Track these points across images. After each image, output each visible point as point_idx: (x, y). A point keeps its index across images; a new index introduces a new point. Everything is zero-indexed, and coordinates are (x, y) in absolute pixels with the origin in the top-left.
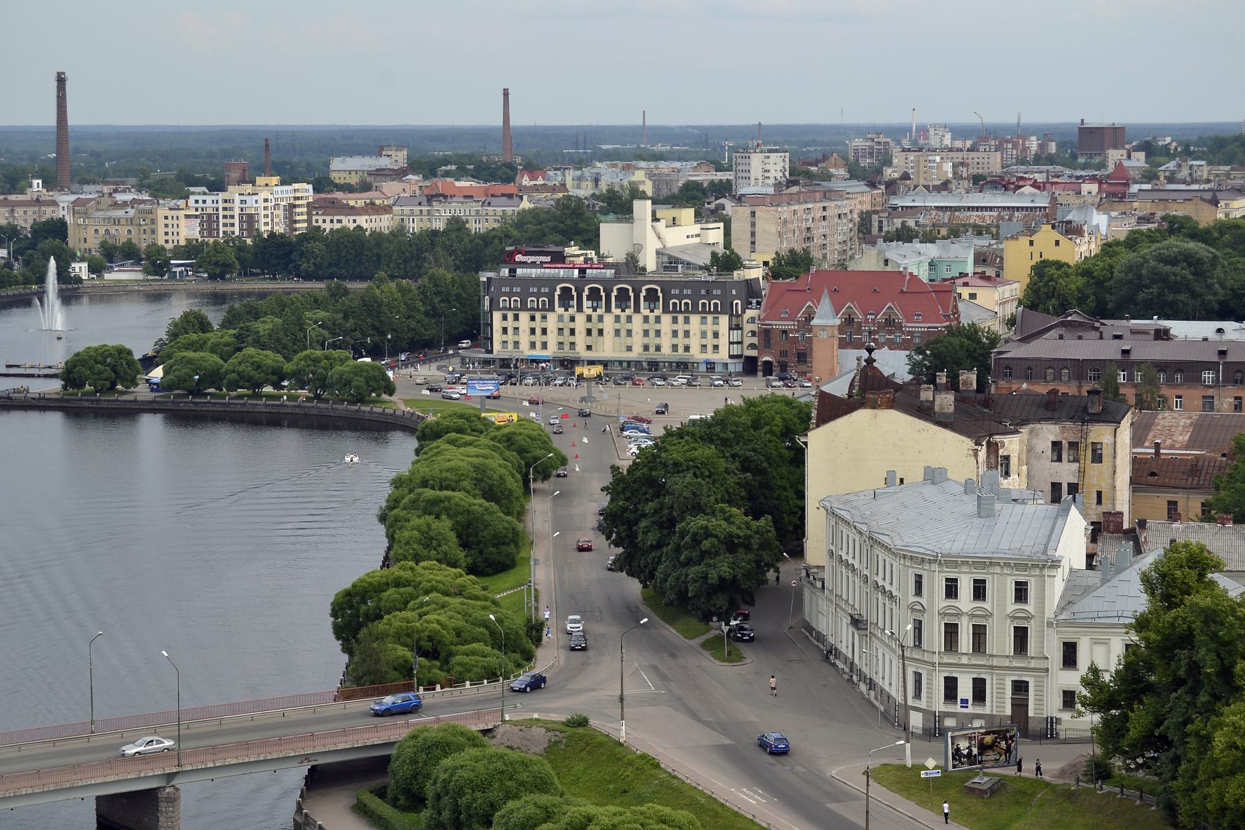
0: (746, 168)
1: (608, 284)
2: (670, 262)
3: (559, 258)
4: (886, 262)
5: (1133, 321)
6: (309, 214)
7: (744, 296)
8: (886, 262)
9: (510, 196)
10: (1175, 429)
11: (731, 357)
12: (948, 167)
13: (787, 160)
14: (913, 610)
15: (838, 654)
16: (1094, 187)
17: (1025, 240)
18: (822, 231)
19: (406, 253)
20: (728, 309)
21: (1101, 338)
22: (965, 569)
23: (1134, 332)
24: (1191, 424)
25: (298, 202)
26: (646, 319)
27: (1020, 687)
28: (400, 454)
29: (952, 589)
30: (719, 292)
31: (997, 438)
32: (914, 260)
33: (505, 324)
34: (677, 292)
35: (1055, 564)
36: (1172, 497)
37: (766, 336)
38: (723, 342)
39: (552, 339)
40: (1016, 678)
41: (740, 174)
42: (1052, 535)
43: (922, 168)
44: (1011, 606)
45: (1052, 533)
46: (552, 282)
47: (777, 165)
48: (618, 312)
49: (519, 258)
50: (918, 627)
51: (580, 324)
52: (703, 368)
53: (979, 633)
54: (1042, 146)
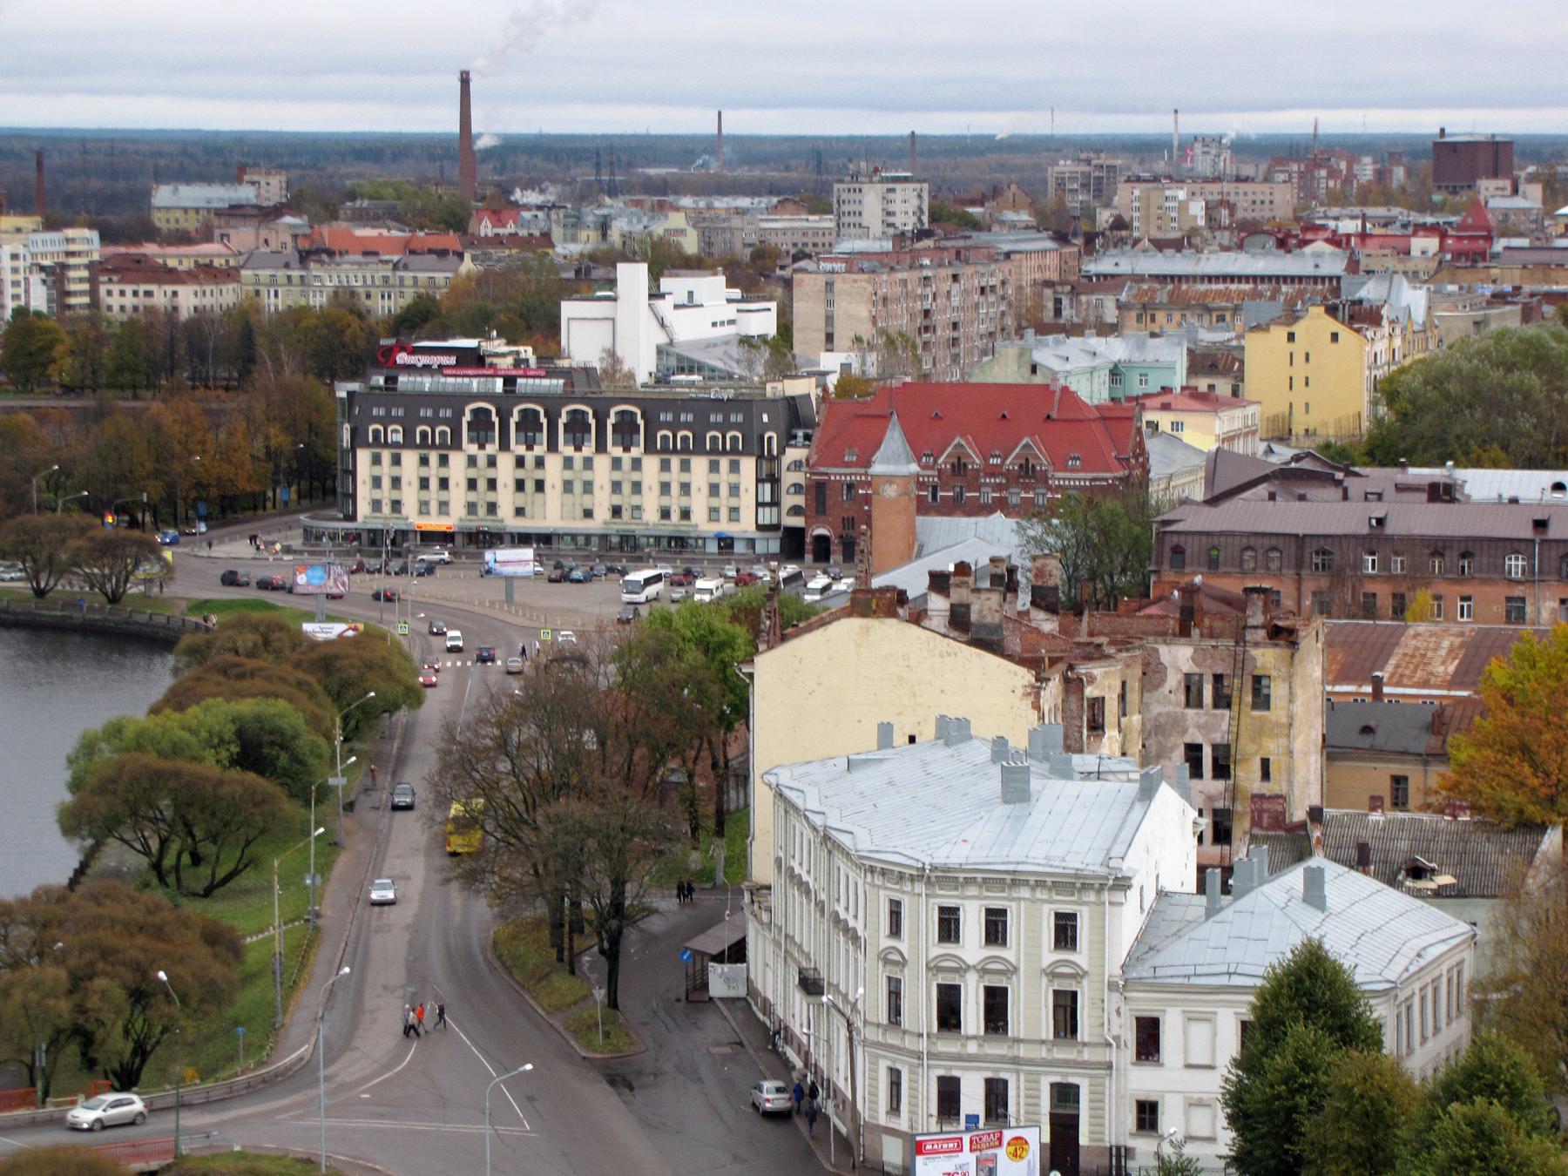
0: (856, 208)
1: (552, 404)
2: (674, 361)
3: (473, 360)
4: (1034, 369)
5: (1412, 471)
6: (93, 281)
7: (783, 426)
8: (1034, 369)
9: (442, 253)
10: (1428, 657)
11: (760, 528)
12: (1197, 209)
13: (925, 195)
14: (886, 962)
15: (789, 1038)
16: (1432, 244)
17: (1279, 333)
18: (951, 316)
19: (224, 352)
20: (754, 445)
21: (1345, 497)
22: (972, 891)
23: (1400, 488)
24: (1462, 645)
25: (72, 261)
26: (616, 463)
27: (1065, 1094)
28: (131, 696)
29: (949, 925)
30: (740, 418)
31: (1082, 670)
32: (1079, 366)
33: (376, 471)
34: (670, 417)
35: (1122, 884)
36: (1397, 769)
37: (818, 493)
38: (747, 502)
39: (458, 496)
40: (1057, 1079)
41: (845, 220)
42: (1124, 832)
43: (1154, 211)
44: (1049, 955)
45: (1120, 829)
46: (457, 400)
47: (909, 205)
48: (617, 451)
49: (402, 358)
50: (895, 995)
51: (505, 471)
52: (712, 547)
53: (996, 1003)
54: (1382, 175)
